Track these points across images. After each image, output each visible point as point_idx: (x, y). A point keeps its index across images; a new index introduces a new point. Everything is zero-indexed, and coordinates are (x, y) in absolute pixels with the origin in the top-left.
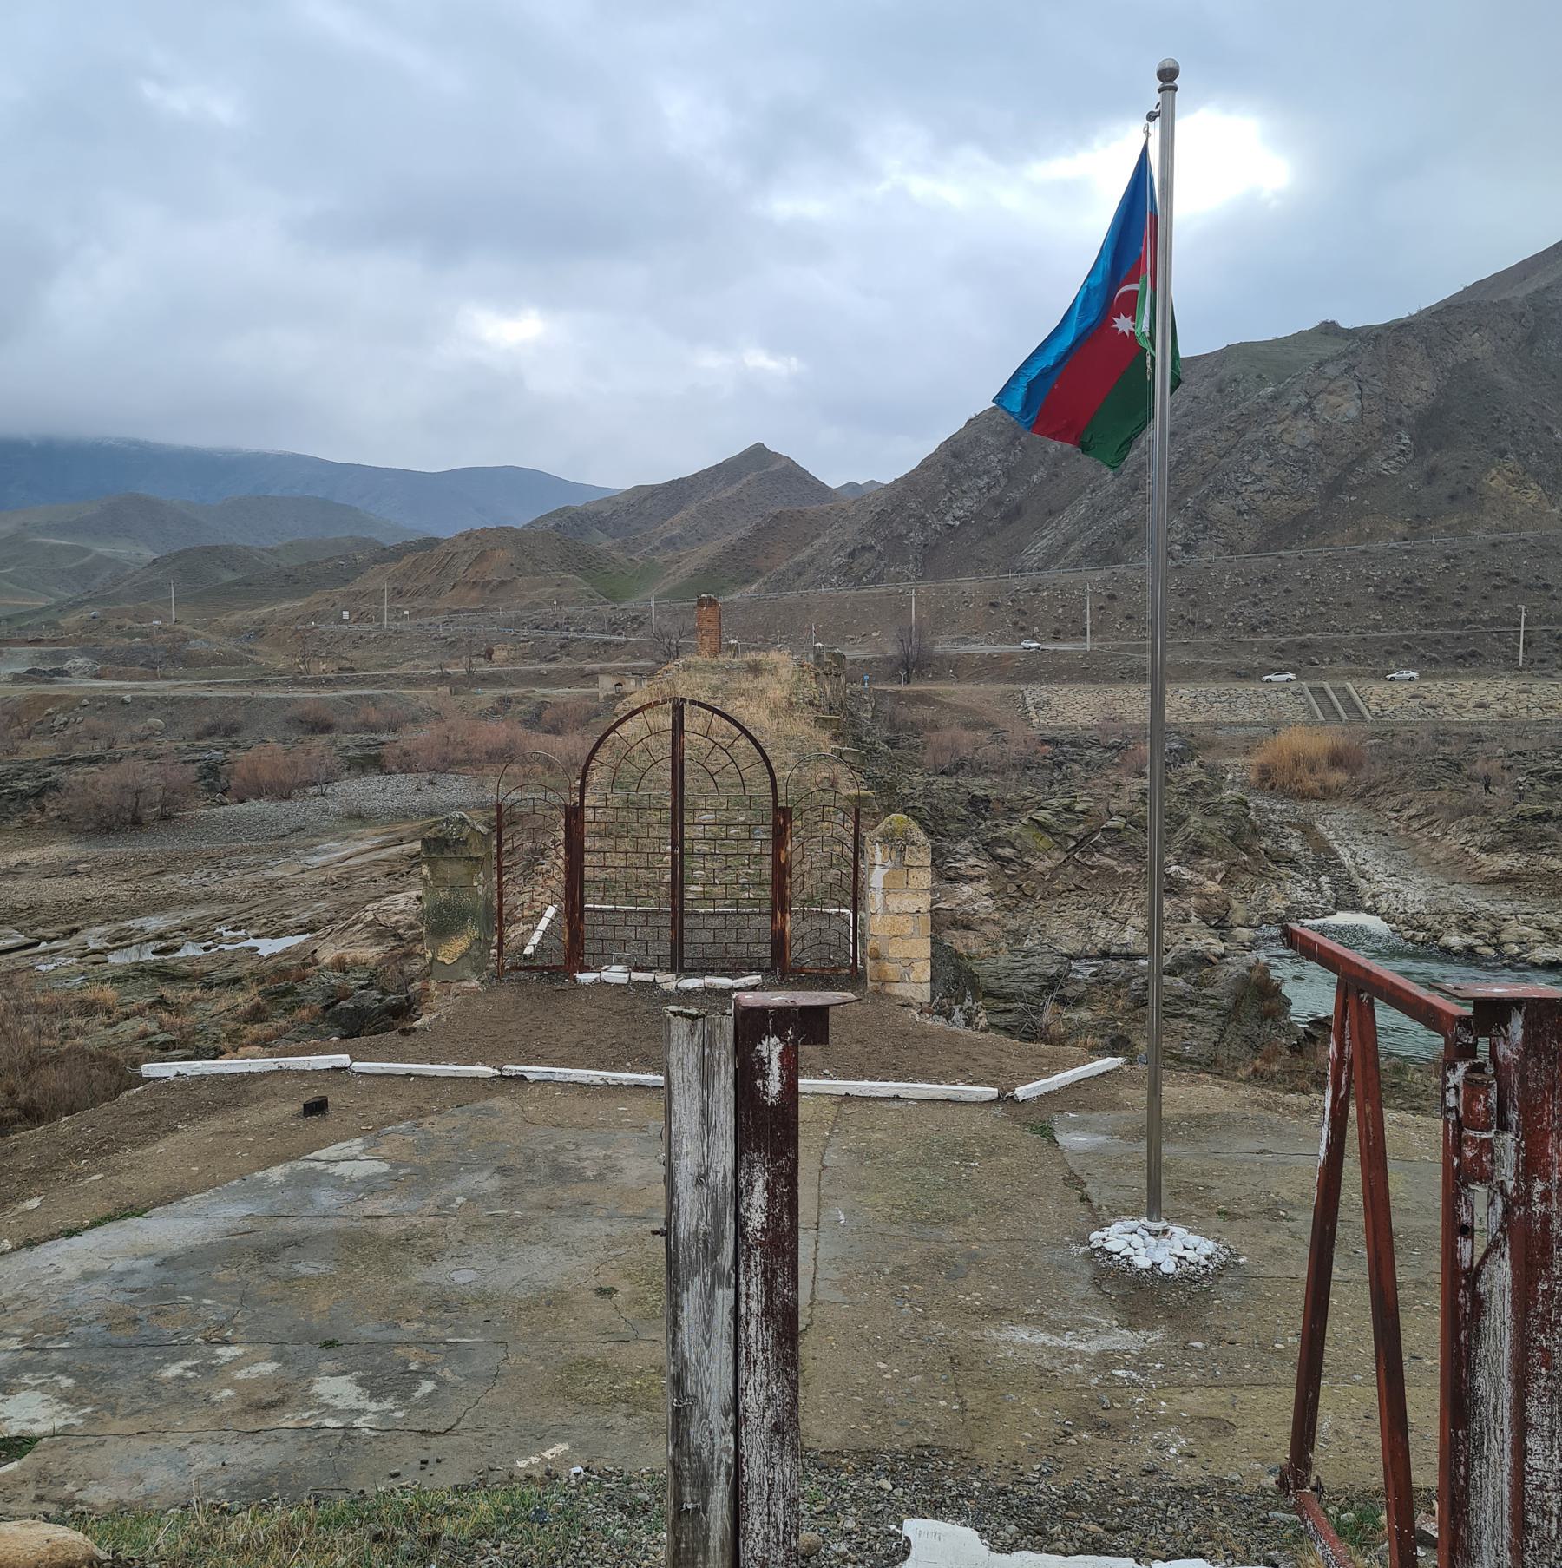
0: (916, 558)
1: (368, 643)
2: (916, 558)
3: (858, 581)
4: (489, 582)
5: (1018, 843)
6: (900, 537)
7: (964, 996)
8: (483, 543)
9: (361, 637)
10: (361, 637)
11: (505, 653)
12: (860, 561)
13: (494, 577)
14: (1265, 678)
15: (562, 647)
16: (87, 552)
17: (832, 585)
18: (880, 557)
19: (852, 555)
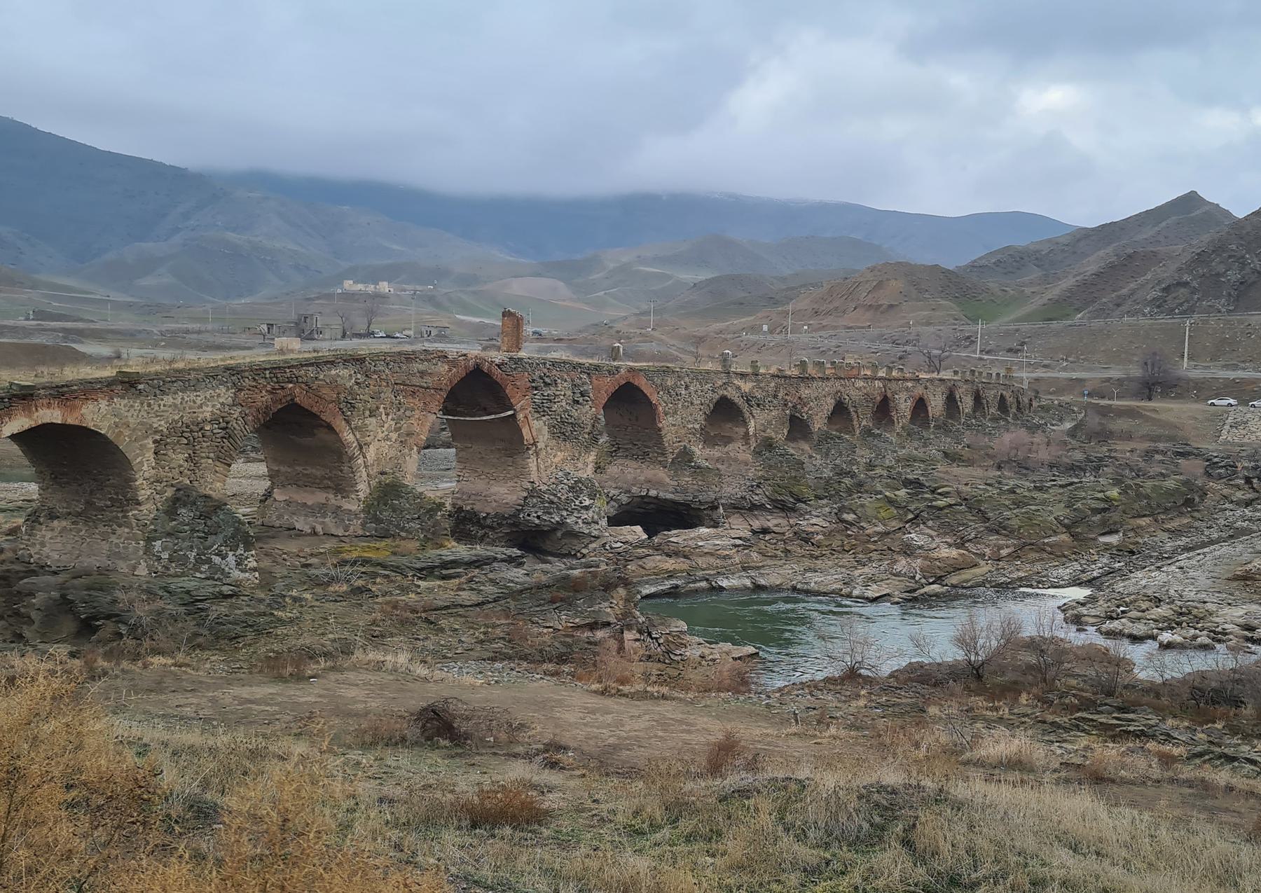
0: (1230, 294)
2: (1230, 294)
3: (1171, 312)
4: (881, 305)
5: (859, 511)
6: (1218, 275)
12: (1174, 295)
13: (885, 302)
14: (1210, 402)
15: (900, 358)
17: (1144, 315)
18: (1193, 293)
19: (1166, 290)
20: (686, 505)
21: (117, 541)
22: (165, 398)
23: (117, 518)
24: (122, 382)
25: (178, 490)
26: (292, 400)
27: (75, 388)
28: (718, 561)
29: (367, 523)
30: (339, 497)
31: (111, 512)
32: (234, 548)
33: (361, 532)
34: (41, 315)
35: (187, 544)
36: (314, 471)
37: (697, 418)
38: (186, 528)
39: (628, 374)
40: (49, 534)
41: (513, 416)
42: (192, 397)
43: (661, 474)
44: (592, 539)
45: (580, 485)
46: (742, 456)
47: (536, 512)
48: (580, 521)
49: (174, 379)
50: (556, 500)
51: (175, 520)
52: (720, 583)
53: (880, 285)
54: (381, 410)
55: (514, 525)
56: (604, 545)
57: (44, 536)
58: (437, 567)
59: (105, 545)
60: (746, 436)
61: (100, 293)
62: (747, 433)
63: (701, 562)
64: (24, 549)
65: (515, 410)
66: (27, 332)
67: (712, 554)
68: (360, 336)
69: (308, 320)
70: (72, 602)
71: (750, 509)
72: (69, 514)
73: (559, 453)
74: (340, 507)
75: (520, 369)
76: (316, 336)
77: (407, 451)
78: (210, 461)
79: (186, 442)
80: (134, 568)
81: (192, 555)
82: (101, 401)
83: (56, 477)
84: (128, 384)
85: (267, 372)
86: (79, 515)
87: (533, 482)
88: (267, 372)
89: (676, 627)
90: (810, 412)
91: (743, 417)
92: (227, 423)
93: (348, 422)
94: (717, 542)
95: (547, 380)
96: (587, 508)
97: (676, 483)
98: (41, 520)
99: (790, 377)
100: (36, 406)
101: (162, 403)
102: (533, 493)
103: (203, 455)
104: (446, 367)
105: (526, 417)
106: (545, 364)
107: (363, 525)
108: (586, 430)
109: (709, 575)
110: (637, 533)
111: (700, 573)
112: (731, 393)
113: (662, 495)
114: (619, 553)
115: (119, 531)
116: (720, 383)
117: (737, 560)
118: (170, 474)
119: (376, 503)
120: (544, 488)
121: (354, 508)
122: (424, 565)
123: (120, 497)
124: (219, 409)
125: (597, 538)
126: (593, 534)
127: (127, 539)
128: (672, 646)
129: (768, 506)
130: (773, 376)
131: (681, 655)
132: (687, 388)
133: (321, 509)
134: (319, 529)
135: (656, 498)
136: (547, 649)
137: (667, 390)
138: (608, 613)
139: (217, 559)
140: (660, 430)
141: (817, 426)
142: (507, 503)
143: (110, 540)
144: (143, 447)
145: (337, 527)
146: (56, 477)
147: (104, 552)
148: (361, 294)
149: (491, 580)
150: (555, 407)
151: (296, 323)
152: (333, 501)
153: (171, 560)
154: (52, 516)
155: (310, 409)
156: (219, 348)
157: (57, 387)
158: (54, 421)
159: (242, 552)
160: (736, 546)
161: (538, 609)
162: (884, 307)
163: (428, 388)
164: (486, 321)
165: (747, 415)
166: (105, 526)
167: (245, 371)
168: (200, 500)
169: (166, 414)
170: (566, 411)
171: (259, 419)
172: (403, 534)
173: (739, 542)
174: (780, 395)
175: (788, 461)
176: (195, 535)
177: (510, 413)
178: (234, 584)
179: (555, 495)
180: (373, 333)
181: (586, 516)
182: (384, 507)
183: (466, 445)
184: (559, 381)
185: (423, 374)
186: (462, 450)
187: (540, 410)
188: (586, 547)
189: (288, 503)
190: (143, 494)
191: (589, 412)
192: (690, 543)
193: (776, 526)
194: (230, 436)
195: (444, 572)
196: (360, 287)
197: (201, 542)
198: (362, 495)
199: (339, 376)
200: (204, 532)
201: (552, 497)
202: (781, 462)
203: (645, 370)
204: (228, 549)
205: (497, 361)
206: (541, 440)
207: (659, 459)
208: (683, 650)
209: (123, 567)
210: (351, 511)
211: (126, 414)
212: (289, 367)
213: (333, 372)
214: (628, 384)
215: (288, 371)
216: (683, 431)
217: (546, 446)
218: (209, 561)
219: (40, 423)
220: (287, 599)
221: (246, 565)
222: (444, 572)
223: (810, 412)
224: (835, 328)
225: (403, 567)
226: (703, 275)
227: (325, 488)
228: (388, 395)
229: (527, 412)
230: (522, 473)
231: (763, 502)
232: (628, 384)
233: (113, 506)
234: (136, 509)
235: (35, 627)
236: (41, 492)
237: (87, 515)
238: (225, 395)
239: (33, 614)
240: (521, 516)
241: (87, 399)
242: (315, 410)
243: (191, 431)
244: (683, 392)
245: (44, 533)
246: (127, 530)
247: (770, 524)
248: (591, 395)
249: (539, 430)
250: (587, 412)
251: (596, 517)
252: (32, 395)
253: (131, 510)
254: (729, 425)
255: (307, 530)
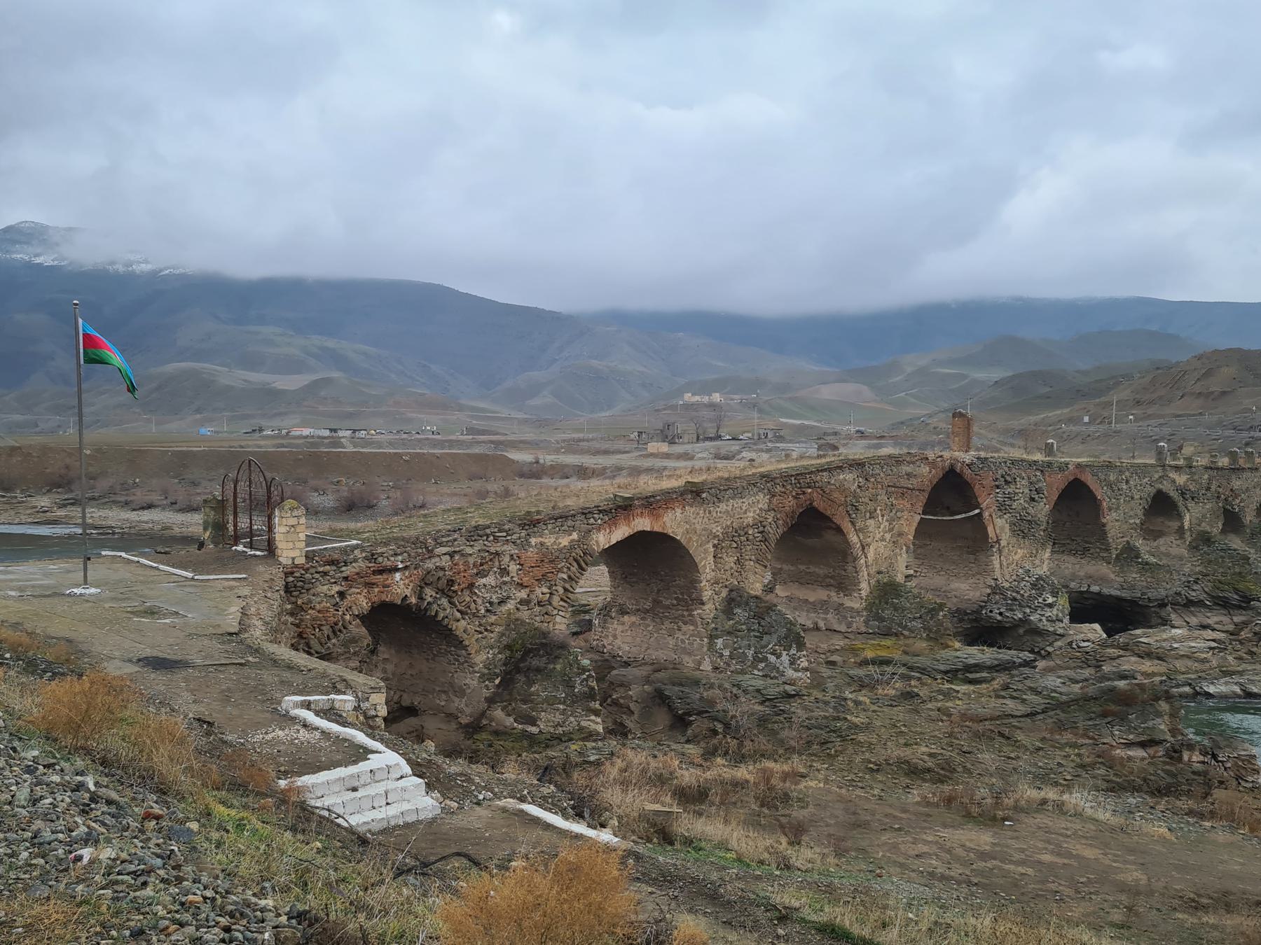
1: (1093, 439)
4: (1212, 393)
7: (791, 647)
8: (1212, 362)
9: (1089, 436)
10: (1089, 436)
11: (1192, 449)
13: (1216, 389)
16: (964, 377)
20: (1133, 603)
21: (683, 637)
22: (721, 505)
23: (683, 616)
24: (692, 492)
25: (731, 591)
26: (811, 504)
27: (658, 498)
28: (1196, 664)
29: (869, 621)
30: (842, 595)
31: (678, 610)
32: (788, 648)
33: (863, 629)
34: (471, 431)
35: (745, 642)
36: (817, 570)
37: (1136, 513)
38: (744, 627)
39: (1077, 471)
40: (620, 628)
41: (980, 515)
42: (740, 504)
43: (1104, 569)
44: (1058, 637)
45: (1042, 582)
46: (1175, 551)
47: (999, 609)
48: (1044, 618)
49: (726, 488)
50: (1019, 597)
51: (733, 619)
52: (1205, 689)
53: (1208, 373)
54: (878, 512)
55: (976, 620)
56: (1070, 644)
57: (616, 629)
58: (960, 670)
59: (671, 642)
60: (1181, 531)
61: (505, 413)
62: (1181, 528)
63: (1179, 664)
64: (598, 639)
65: (981, 509)
66: (459, 443)
67: (1188, 657)
68: (711, 439)
69: (671, 427)
70: (669, 697)
71: (1185, 606)
72: (638, 610)
73: (1019, 551)
74: (843, 604)
75: (986, 469)
76: (677, 440)
77: (898, 550)
78: (752, 563)
79: (735, 545)
80: (700, 663)
81: (750, 653)
82: (677, 510)
83: (626, 577)
84: (694, 493)
85: (793, 478)
86: (648, 611)
87: (996, 579)
88: (793, 478)
89: (1244, 750)
90: (1242, 504)
91: (1178, 511)
92: (764, 527)
93: (853, 523)
94: (1193, 644)
95: (1008, 479)
96: (1051, 606)
97: (1122, 580)
98: (613, 615)
99: (1222, 469)
100: (633, 516)
101: (719, 510)
102: (996, 590)
103: (747, 557)
104: (928, 469)
105: (991, 516)
106: (1005, 462)
107: (866, 622)
108: (1042, 528)
109: (1191, 679)
110: (1095, 631)
111: (1181, 677)
112: (1166, 487)
113: (1106, 591)
114: (1088, 653)
115: (684, 628)
116: (1157, 476)
117: (1214, 663)
118: (724, 576)
119: (877, 602)
120: (1006, 585)
121: (856, 605)
122: (948, 668)
123: (686, 597)
124: (758, 515)
125: (1062, 636)
126: (1058, 632)
127: (692, 635)
128: (1243, 772)
129: (1208, 603)
130: (1206, 468)
131: (1253, 782)
132: (1127, 482)
133: (823, 606)
134: (821, 624)
135: (1099, 594)
136: (1152, 778)
137: (1110, 485)
138: (1162, 730)
139: (772, 658)
140: (1104, 525)
141: (1248, 519)
142: (970, 600)
143: (676, 636)
144: (706, 551)
145: (840, 623)
146: (626, 577)
147: (671, 646)
148: (698, 404)
149: (1031, 688)
150: (1015, 505)
151: (661, 431)
152: (836, 599)
153: (731, 657)
154: (623, 612)
155: (824, 512)
156: (606, 452)
157: (647, 497)
158: (645, 529)
159: (795, 652)
160: (1211, 648)
161: (1090, 723)
162: (1216, 393)
163: (914, 489)
164: (806, 423)
165: (1182, 508)
166: (671, 623)
167: (777, 478)
168: (752, 600)
169: (722, 520)
170: (1025, 508)
171: (787, 523)
172: (906, 633)
173: (1214, 644)
174: (1213, 487)
175: (1231, 557)
176: (752, 634)
177: (977, 511)
178: (789, 682)
179: (1018, 592)
180: (720, 437)
181: (1050, 614)
182: (885, 606)
183: (925, 542)
184: (1018, 479)
185: (909, 475)
186: (921, 547)
187: (1003, 508)
188: (1051, 644)
189: (790, 599)
190: (707, 594)
191: (1042, 510)
192: (1164, 644)
193: (1217, 623)
194: (766, 540)
195: (971, 676)
196: (697, 398)
197: (758, 642)
198: (864, 593)
199: (846, 480)
200: (759, 632)
201: (1014, 594)
202: (1223, 557)
203: (1090, 465)
204: (782, 648)
205: (967, 462)
206: (1003, 538)
207: (1101, 554)
208: (1256, 776)
209: (689, 662)
210: (853, 608)
211: (694, 521)
212: (809, 473)
213: (841, 477)
214: (1076, 479)
215: (808, 476)
216: (1125, 527)
217: (1008, 544)
218: (765, 659)
219: (636, 531)
220: (849, 703)
221: (799, 665)
222: (971, 676)
223: (1242, 504)
224: (1162, 416)
225: (929, 669)
226: (996, 374)
227: (827, 586)
228: (883, 497)
229: (992, 510)
230: (986, 570)
231: (1202, 598)
232: (1076, 479)
233: (679, 604)
234: (701, 609)
235: (636, 716)
236: (613, 589)
237: (655, 612)
238: (762, 500)
239: (632, 705)
240: (984, 612)
241: (667, 508)
242: (828, 513)
243: (739, 536)
244: (1125, 487)
245: (614, 626)
246: (692, 628)
247: (1210, 621)
248: (1045, 493)
249: (1002, 528)
250: (1042, 509)
251: (1060, 615)
252: (631, 506)
253: (696, 609)
254: (1160, 520)
255: (809, 624)
